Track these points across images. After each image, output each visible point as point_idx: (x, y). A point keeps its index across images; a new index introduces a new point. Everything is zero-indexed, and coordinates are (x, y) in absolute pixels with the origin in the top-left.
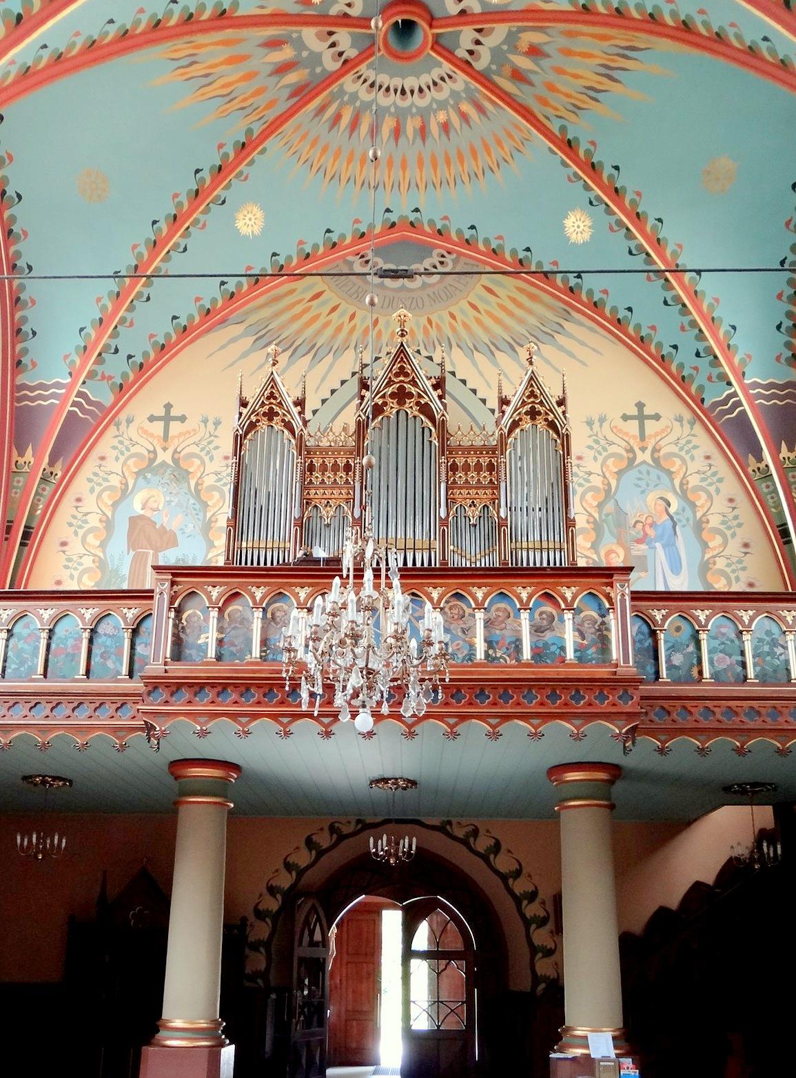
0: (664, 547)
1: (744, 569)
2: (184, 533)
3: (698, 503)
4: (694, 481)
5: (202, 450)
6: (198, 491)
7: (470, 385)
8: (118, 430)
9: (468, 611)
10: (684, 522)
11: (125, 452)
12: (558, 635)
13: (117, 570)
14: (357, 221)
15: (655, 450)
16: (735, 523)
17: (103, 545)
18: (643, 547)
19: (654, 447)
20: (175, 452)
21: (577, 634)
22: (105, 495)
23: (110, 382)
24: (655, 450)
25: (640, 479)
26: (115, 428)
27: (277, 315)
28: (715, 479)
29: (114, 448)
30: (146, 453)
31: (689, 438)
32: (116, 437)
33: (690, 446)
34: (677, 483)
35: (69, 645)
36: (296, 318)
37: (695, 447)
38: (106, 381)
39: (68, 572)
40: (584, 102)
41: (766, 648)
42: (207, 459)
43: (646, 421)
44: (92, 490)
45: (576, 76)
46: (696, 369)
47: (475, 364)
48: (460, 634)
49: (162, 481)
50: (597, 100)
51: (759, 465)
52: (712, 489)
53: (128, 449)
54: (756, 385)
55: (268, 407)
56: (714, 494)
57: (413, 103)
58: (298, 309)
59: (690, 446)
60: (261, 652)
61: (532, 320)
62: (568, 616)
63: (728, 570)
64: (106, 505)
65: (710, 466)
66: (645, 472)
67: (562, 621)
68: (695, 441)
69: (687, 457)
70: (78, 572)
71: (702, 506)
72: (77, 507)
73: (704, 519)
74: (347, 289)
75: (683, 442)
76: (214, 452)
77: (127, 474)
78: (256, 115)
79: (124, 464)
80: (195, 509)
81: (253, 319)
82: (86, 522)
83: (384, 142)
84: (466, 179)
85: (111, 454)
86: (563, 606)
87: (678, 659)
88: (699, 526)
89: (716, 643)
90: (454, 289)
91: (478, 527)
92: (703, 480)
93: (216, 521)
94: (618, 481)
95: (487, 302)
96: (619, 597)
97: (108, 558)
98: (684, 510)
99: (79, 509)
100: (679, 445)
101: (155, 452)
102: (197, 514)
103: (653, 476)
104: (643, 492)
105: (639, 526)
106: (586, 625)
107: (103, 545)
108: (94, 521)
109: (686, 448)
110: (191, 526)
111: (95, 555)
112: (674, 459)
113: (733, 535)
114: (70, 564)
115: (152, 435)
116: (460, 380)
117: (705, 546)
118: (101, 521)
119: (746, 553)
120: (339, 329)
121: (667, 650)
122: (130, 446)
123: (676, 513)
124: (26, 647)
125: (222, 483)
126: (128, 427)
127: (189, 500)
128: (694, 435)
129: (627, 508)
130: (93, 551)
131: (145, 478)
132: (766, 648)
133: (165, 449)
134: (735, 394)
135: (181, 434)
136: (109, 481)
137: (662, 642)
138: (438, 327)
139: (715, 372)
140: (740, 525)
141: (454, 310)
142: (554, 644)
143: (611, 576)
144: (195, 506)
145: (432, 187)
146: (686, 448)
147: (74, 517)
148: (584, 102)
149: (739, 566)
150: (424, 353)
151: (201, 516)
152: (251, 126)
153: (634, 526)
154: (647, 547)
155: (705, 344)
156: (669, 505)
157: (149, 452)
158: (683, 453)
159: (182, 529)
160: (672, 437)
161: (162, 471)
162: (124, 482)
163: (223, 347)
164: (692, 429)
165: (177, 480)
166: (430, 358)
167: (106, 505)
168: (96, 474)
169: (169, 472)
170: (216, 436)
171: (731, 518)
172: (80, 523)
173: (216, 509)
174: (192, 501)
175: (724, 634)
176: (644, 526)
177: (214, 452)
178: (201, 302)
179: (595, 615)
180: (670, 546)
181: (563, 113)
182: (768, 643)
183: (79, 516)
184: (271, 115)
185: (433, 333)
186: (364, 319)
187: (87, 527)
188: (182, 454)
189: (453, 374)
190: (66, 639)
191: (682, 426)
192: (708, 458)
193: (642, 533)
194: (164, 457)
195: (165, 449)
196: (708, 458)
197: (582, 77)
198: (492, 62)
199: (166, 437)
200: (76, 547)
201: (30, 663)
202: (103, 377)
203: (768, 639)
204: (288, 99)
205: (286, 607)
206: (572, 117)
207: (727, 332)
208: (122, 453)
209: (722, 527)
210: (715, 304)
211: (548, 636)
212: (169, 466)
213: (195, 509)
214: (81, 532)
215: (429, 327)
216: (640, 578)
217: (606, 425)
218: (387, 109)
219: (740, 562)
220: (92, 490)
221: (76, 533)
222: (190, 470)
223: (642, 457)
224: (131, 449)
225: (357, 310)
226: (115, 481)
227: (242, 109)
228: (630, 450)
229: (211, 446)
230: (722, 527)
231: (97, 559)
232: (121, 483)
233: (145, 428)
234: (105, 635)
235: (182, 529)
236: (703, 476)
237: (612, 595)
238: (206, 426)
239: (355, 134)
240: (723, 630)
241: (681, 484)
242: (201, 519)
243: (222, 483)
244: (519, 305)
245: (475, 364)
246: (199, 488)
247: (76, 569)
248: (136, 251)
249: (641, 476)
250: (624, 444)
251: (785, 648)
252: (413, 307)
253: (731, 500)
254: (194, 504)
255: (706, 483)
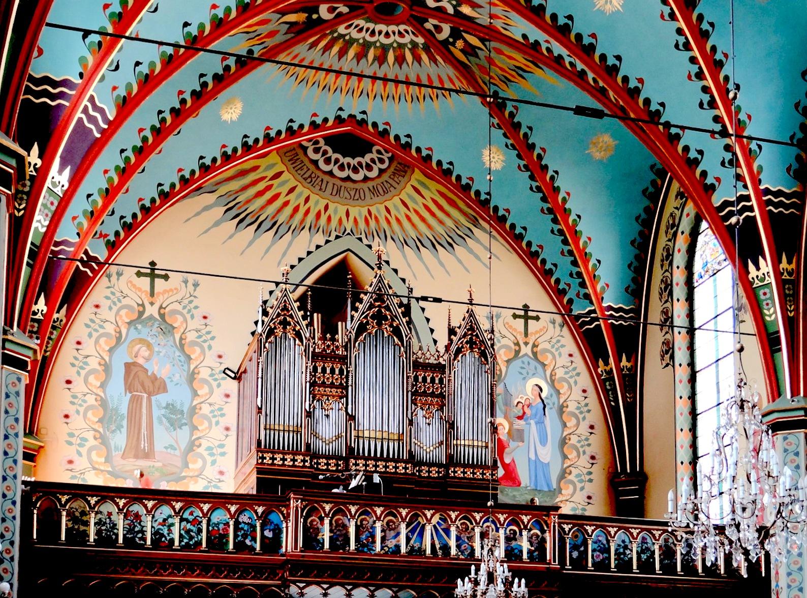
0: (536, 423)
1: (589, 445)
2: (172, 381)
3: (561, 391)
4: (560, 373)
5: (184, 308)
6: (182, 346)
7: (401, 275)
8: (110, 281)
9: (470, 526)
10: (551, 405)
11: (117, 303)
12: (519, 543)
13: (116, 409)
14: (315, 115)
15: (535, 346)
16: (586, 409)
17: (103, 386)
18: (522, 422)
19: (534, 343)
20: (161, 307)
21: (529, 543)
22: (102, 341)
23: (106, 239)
24: (535, 346)
25: (522, 368)
26: (107, 279)
27: (244, 188)
28: (574, 373)
29: (107, 298)
30: (136, 306)
31: (559, 338)
32: (108, 287)
33: (559, 344)
34: (548, 373)
35: (221, 529)
36: (260, 194)
37: (563, 346)
38: (102, 238)
39: (74, 407)
40: (513, 76)
41: (622, 550)
42: (188, 316)
43: (529, 321)
44: (90, 335)
45: (510, 58)
46: (569, 285)
47: (405, 256)
48: (466, 540)
49: (151, 333)
50: (524, 78)
51: (606, 367)
52: (572, 381)
53: (120, 301)
54: (610, 308)
55: (283, 317)
56: (573, 385)
57: (378, 40)
58: (261, 186)
59: (559, 344)
60: (355, 546)
61: (449, 223)
62: (525, 533)
63: (579, 445)
64: (104, 350)
65: (572, 362)
66: (526, 363)
67: (521, 535)
68: (563, 341)
69: (556, 354)
70: (83, 408)
71: (564, 394)
72: (78, 350)
73: (565, 405)
74: (302, 172)
75: (554, 341)
76: (194, 311)
77: (120, 324)
78: (258, 40)
79: (117, 313)
80: (180, 361)
81: (223, 189)
82: (86, 364)
83: (348, 61)
84: (409, 99)
85: (105, 304)
86: (522, 527)
87: (575, 554)
88: (561, 409)
89: (596, 546)
90: (389, 185)
91: (431, 426)
92: (566, 373)
93: (198, 373)
94: (507, 367)
95: (416, 203)
96: (552, 524)
97: (108, 398)
98: (551, 396)
99: (79, 351)
100: (552, 343)
101: (143, 305)
102: (183, 366)
103: (532, 367)
104: (524, 378)
105: (520, 405)
106: (534, 538)
107: (103, 386)
108: (94, 363)
109: (556, 346)
110: (177, 375)
111: (96, 395)
112: (547, 354)
113: (584, 418)
114: (76, 401)
115: (140, 290)
116: (393, 269)
117: (565, 425)
118: (100, 364)
119: (591, 433)
120: (296, 209)
121: (570, 549)
122: (121, 298)
123: (547, 398)
124: (192, 528)
125: (202, 339)
126: (118, 279)
127: (175, 352)
128: (562, 336)
129: (512, 390)
130: (95, 390)
131: (136, 328)
132: (622, 550)
133: (152, 304)
134: (594, 311)
135: (165, 291)
136: (104, 328)
137: (568, 544)
138: (376, 218)
139: (583, 291)
140: (589, 411)
141: (389, 204)
142: (516, 549)
143: (549, 512)
144: (180, 358)
145: (380, 97)
146: (556, 346)
147: (76, 358)
148: (513, 76)
149: (586, 443)
150: (365, 241)
151: (185, 367)
152: (253, 48)
153: (517, 406)
154: (525, 423)
155: (578, 269)
156: (541, 390)
157: (138, 305)
158: (553, 350)
159: (170, 378)
160: (547, 337)
161: (150, 324)
162: (118, 330)
163: (198, 214)
164: (561, 331)
165: (164, 333)
166: (370, 247)
167: (104, 350)
168: (92, 321)
169: (156, 325)
170: (195, 297)
171: (583, 405)
172: (81, 364)
173: (198, 362)
174: (178, 353)
175: (600, 541)
176: (523, 406)
177: (194, 311)
178: (183, 173)
179: (539, 533)
180: (540, 423)
181: (497, 82)
182: (623, 547)
183: (80, 358)
184: (270, 42)
185: (373, 223)
186: (317, 203)
187: (88, 368)
188: (167, 309)
189: (387, 262)
190: (218, 524)
191: (554, 327)
192: (571, 355)
193: (522, 412)
194: (152, 311)
195: (152, 304)
196: (571, 355)
197: (514, 59)
198: (450, 36)
199: (152, 294)
200: (79, 386)
201: (196, 539)
202: (101, 235)
203: (623, 545)
204: (285, 34)
205: (368, 518)
206: (504, 86)
207: (595, 265)
208: (115, 304)
209: (577, 412)
210: (588, 242)
211: (514, 544)
212: (156, 320)
213: (180, 361)
214: (83, 373)
215: (369, 218)
216: (518, 447)
217: (500, 320)
218: (357, 40)
219: (587, 439)
220: (90, 335)
221: (78, 373)
222: (175, 325)
223: (526, 350)
224: (123, 300)
225: (311, 194)
226: (110, 328)
227: (247, 33)
228: (517, 344)
229: (192, 305)
230: (577, 412)
231: (99, 398)
232: (116, 332)
233: (134, 283)
234: (243, 522)
235: (170, 378)
236: (566, 370)
237: (549, 522)
238: (186, 287)
239: (327, 53)
240: (600, 538)
241: (551, 375)
242: (186, 370)
243: (202, 339)
244: (440, 208)
245: (405, 256)
246: (183, 342)
247: (81, 405)
248: (142, 134)
249: (523, 366)
250: (513, 338)
251: (631, 551)
252: (356, 198)
253: (584, 391)
254: (179, 356)
255: (568, 375)
